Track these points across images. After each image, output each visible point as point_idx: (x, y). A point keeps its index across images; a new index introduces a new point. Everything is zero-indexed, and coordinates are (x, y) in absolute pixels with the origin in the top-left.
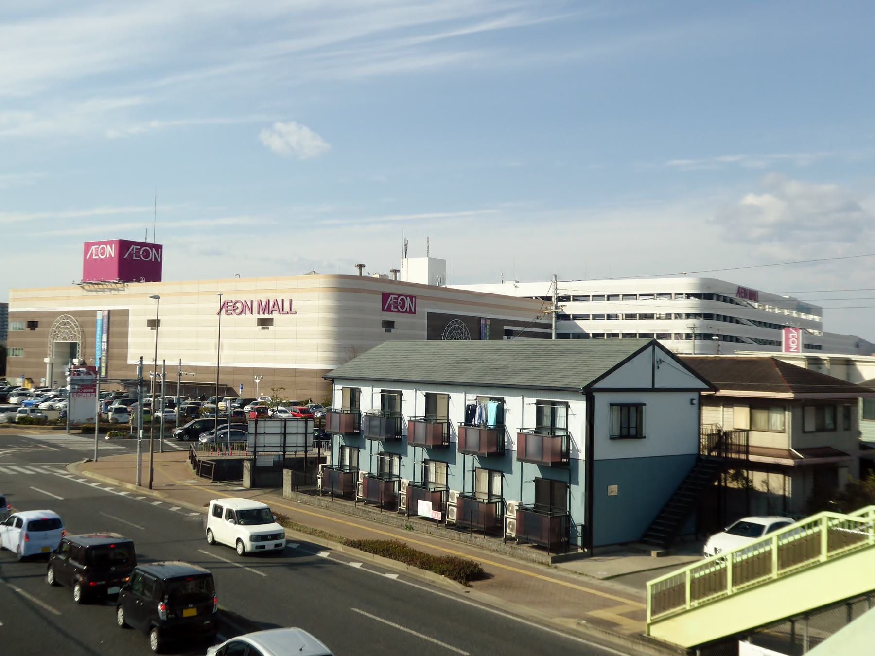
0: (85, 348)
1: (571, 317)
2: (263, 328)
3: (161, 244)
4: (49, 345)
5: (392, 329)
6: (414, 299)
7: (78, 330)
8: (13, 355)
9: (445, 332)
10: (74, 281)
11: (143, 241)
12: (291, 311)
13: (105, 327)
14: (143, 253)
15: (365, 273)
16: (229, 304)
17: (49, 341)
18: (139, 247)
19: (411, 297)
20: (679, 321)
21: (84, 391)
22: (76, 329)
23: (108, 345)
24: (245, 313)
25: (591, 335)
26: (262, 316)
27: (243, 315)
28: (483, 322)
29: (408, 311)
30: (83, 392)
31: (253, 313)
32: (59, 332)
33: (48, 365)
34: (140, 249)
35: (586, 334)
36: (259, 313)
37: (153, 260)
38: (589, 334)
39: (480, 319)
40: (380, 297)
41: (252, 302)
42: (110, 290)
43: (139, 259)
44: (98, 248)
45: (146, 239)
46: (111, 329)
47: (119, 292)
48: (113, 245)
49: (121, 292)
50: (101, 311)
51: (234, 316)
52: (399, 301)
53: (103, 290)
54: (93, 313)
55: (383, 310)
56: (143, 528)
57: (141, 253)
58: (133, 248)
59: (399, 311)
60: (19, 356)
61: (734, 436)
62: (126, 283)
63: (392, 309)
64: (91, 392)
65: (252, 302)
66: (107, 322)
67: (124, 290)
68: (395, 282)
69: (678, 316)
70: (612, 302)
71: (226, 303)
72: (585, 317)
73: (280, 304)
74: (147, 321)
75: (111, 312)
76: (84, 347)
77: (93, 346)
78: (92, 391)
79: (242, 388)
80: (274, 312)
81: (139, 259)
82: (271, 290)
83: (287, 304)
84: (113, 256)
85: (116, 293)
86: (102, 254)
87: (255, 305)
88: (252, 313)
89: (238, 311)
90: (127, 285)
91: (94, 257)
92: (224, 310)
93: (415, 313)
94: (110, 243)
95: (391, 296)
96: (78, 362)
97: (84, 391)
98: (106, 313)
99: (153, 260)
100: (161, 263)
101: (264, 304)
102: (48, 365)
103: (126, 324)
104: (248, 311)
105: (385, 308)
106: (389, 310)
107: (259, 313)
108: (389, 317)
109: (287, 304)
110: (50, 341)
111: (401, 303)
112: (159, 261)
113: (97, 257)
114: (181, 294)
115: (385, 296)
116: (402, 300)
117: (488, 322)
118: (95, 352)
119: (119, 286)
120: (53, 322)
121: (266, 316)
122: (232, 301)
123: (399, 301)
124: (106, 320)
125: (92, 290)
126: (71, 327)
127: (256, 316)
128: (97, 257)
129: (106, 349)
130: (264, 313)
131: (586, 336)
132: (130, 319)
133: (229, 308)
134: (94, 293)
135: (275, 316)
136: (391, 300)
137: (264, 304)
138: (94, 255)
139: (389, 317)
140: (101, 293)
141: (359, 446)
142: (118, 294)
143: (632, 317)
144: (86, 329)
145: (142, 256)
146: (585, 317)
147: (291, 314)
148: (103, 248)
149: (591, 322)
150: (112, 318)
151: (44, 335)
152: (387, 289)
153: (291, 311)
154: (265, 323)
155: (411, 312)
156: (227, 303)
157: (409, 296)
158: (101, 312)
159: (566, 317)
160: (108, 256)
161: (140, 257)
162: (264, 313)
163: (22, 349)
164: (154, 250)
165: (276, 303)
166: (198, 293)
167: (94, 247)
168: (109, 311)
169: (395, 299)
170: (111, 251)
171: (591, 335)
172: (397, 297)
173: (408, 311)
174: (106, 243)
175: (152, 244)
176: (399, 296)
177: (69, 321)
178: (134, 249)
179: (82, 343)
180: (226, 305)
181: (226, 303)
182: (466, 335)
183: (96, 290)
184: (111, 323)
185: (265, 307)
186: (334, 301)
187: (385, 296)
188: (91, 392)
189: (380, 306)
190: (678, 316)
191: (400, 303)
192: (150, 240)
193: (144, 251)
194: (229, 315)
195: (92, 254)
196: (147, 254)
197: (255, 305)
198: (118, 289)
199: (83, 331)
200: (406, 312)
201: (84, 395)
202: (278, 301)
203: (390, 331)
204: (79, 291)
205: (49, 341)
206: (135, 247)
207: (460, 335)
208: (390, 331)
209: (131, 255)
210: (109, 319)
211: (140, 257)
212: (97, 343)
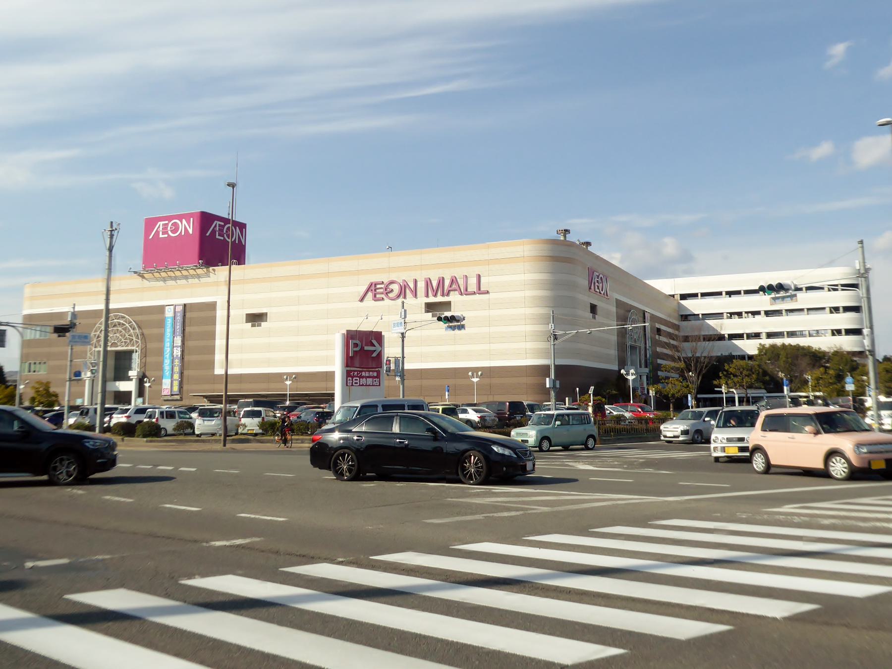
0: (145, 356)
1: (700, 316)
4: (89, 355)
7: (135, 333)
8: (30, 372)
10: (130, 269)
12: (479, 291)
13: (179, 327)
15: (570, 238)
16: (378, 286)
17: (88, 349)
20: (835, 315)
21: (363, 374)
22: (132, 331)
23: (183, 352)
26: (432, 299)
30: (361, 377)
32: (125, 335)
33: (87, 382)
34: (223, 226)
35: (721, 335)
36: (427, 296)
37: (237, 242)
38: (724, 335)
41: (416, 282)
42: (186, 278)
43: (222, 238)
46: (187, 329)
47: (189, 280)
49: (203, 280)
51: (387, 302)
53: (175, 278)
54: (161, 309)
57: (225, 232)
60: (38, 372)
61: (760, 468)
62: (211, 268)
64: (373, 377)
65: (416, 282)
66: (182, 320)
67: (209, 277)
69: (836, 310)
70: (734, 298)
71: (373, 285)
72: (718, 316)
73: (461, 282)
74: (245, 316)
75: (187, 306)
76: (144, 355)
77: (160, 352)
78: (375, 374)
79: (448, 391)
80: (452, 293)
81: (222, 238)
82: (422, 267)
83: (473, 282)
84: (191, 231)
86: (174, 232)
90: (214, 270)
91: (161, 236)
92: (370, 294)
94: (187, 217)
96: (136, 375)
97: (363, 374)
98: (180, 309)
99: (237, 242)
100: (244, 246)
101: (435, 284)
102: (87, 382)
107: (427, 296)
112: (244, 244)
113: (166, 236)
114: (300, 277)
118: (163, 360)
119: (200, 271)
120: (96, 324)
121: (440, 299)
124: (179, 318)
125: (157, 279)
126: (125, 329)
127: (422, 300)
128: (166, 236)
129: (179, 356)
130: (435, 295)
131: (721, 338)
132: (217, 315)
134: (161, 283)
135: (454, 298)
137: (435, 284)
138: (161, 233)
140: (171, 283)
142: (199, 282)
144: (146, 332)
147: (479, 294)
148: (175, 224)
149: (726, 322)
150: (188, 315)
160: (183, 234)
161: (223, 236)
162: (435, 295)
163: (45, 363)
164: (184, 221)
165: (454, 281)
166: (328, 275)
167: (161, 223)
168: (185, 305)
170: (188, 227)
174: (180, 217)
177: (122, 322)
180: (373, 288)
181: (373, 285)
183: (164, 280)
184: (187, 321)
188: (373, 377)
190: (836, 310)
195: (157, 232)
197: (421, 285)
198: (199, 276)
199: (143, 334)
201: (363, 381)
204: (137, 281)
205: (88, 349)
206: (218, 223)
209: (157, 232)
211: (223, 236)
212: (166, 349)
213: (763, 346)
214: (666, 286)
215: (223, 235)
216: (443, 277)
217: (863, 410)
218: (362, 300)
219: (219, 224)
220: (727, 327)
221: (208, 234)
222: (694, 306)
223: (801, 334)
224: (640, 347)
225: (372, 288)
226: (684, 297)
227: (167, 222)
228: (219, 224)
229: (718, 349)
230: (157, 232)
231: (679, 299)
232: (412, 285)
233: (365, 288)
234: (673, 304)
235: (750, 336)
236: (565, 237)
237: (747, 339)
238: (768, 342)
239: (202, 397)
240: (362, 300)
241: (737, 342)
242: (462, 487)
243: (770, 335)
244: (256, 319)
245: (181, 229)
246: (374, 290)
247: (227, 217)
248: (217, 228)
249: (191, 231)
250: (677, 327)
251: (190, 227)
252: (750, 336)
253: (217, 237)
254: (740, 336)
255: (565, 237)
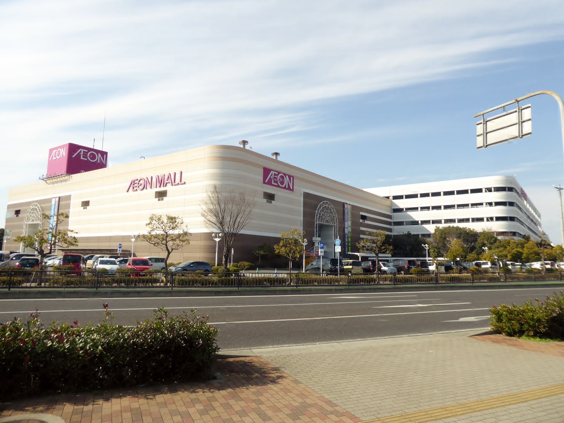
2: (159, 200)
3: (107, 151)
5: (272, 201)
6: (292, 178)
9: (318, 210)
11: (92, 147)
14: (90, 156)
16: (136, 182)
18: (87, 151)
19: (290, 177)
24: (146, 188)
25: (420, 222)
26: (159, 189)
27: (145, 190)
28: (346, 206)
29: (287, 187)
31: (152, 187)
34: (87, 153)
37: (99, 162)
39: (343, 204)
40: (262, 171)
43: (86, 159)
44: (56, 151)
45: (94, 146)
48: (65, 148)
50: (54, 198)
52: (278, 177)
53: (57, 182)
55: (264, 182)
56: (105, 353)
58: (81, 151)
59: (278, 186)
63: (273, 183)
68: (276, 161)
71: (133, 182)
75: (61, 198)
80: (168, 184)
81: (86, 159)
83: (178, 176)
84: (64, 155)
85: (64, 183)
87: (154, 180)
88: (151, 188)
89: (141, 187)
93: (293, 190)
94: (61, 147)
95: (272, 172)
98: (57, 199)
99: (99, 162)
103: (68, 206)
104: (148, 186)
105: (266, 181)
106: (269, 183)
107: (156, 187)
108: (270, 190)
109: (178, 176)
110: (25, 223)
111: (281, 179)
115: (267, 171)
116: (282, 183)
117: (349, 207)
119: (66, 178)
121: (162, 189)
122: (137, 179)
123: (278, 177)
124: (57, 205)
131: (416, 223)
133: (135, 185)
134: (52, 185)
135: (169, 188)
136: (272, 175)
139: (270, 190)
141: (77, 321)
143: (303, 290)
145: (89, 158)
146: (416, 209)
147: (181, 184)
150: (61, 203)
151: (22, 219)
152: (269, 166)
153: (181, 182)
154: (161, 195)
155: (289, 189)
156: (134, 182)
157: (287, 175)
158: (55, 199)
159: (400, 210)
160: (61, 156)
161: (86, 158)
162: (160, 187)
164: (99, 155)
168: (59, 198)
169: (275, 174)
170: (64, 153)
171: (420, 222)
172: (277, 173)
173: (287, 187)
175: (101, 151)
176: (279, 173)
177: (37, 208)
178: (82, 153)
179: (42, 224)
180: (133, 183)
181: (133, 182)
182: (334, 214)
183: (53, 183)
185: (161, 182)
186: (217, 169)
187: (267, 171)
189: (261, 178)
191: (280, 179)
192: (98, 147)
193: (91, 154)
194: (135, 191)
196: (93, 157)
198: (65, 181)
200: (285, 188)
202: (171, 174)
203: (271, 202)
206: (83, 150)
207: (329, 214)
208: (271, 202)
209: (79, 155)
210: (59, 204)
211: (86, 158)
213: (438, 228)
214: (381, 192)
215: (87, 157)
216: (164, 175)
217: (186, 234)
218: (128, 191)
219: (83, 151)
220: (417, 216)
221: (73, 156)
222: (401, 204)
223: (452, 221)
224: (335, 226)
225: (133, 183)
226: (395, 198)
227: (56, 150)
228: (83, 151)
229: (414, 230)
230: (79, 155)
231: (392, 199)
232: (150, 180)
233: (130, 183)
234: (387, 202)
235: (434, 222)
236: (276, 157)
237: (432, 224)
238: (442, 226)
239: (61, 251)
240: (128, 191)
241: (425, 226)
242: (390, 315)
243: (447, 221)
244: (86, 204)
245: (61, 154)
246: (133, 185)
247: (92, 148)
248: (82, 153)
249: (64, 155)
250: (390, 217)
251: (100, 157)
252: (434, 222)
253: (82, 158)
254: (427, 222)
255: (276, 157)
